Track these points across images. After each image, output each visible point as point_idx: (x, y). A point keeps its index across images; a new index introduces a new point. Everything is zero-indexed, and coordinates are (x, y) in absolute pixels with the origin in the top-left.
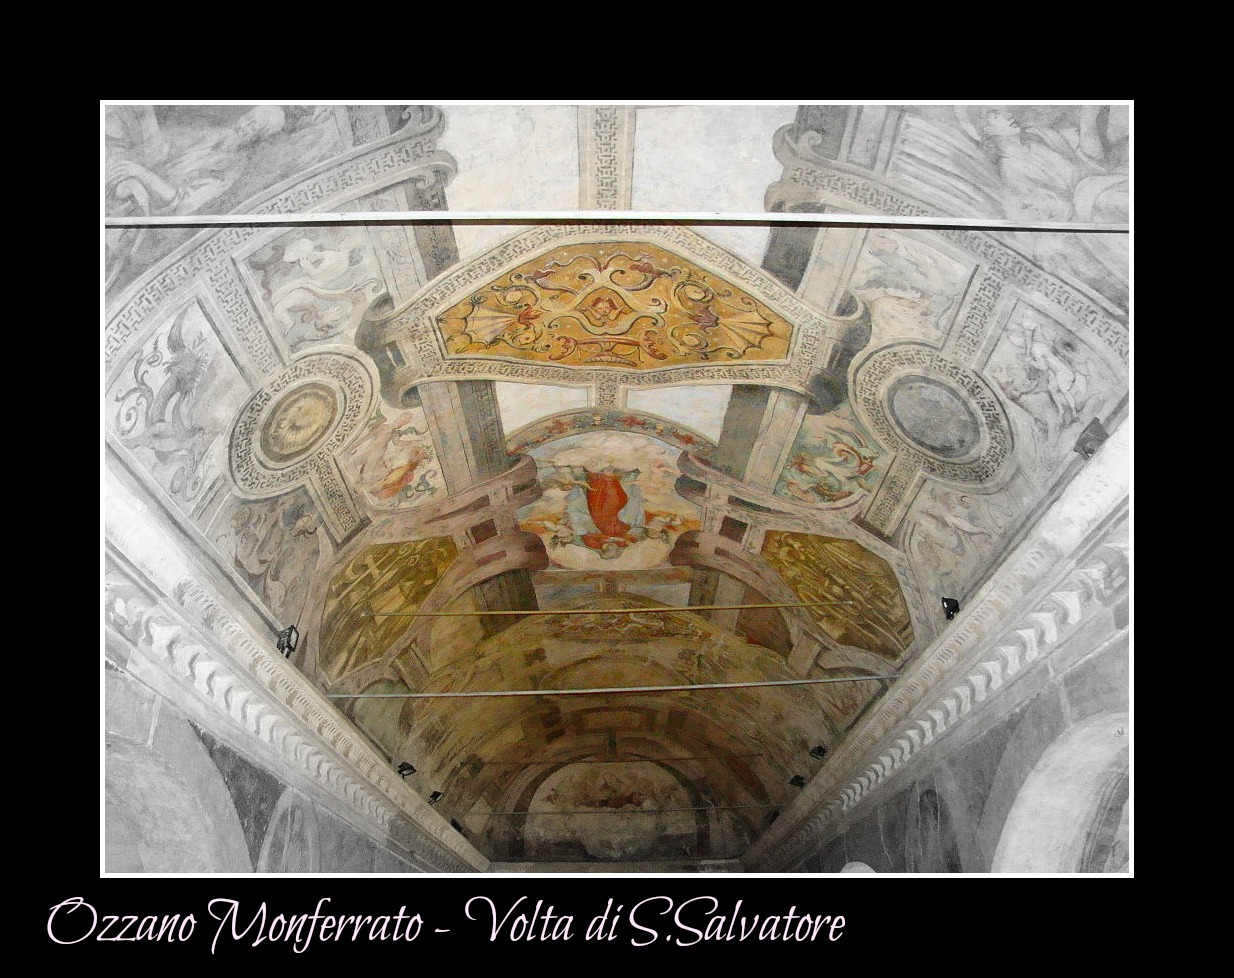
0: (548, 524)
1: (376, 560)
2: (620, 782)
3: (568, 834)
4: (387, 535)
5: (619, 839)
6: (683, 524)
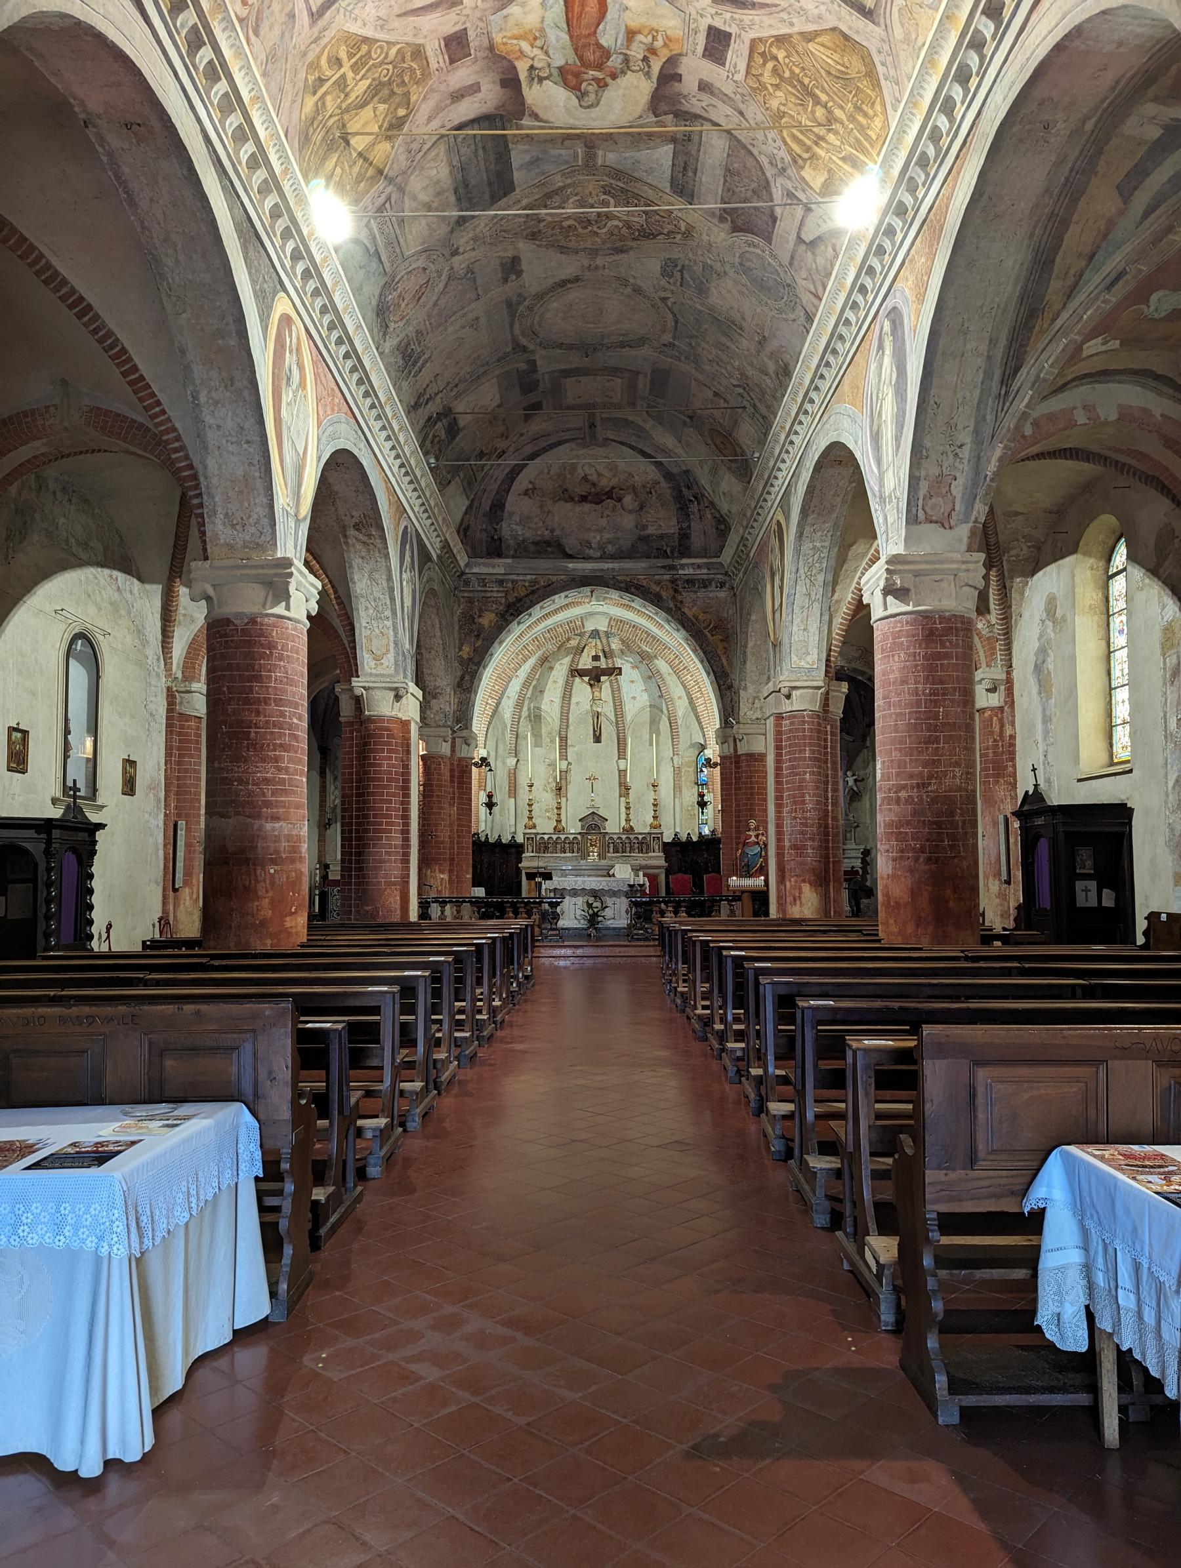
0: (525, 46)
1: (351, 56)
2: (599, 475)
3: (546, 533)
4: (359, 22)
5: (598, 538)
6: (665, 45)
